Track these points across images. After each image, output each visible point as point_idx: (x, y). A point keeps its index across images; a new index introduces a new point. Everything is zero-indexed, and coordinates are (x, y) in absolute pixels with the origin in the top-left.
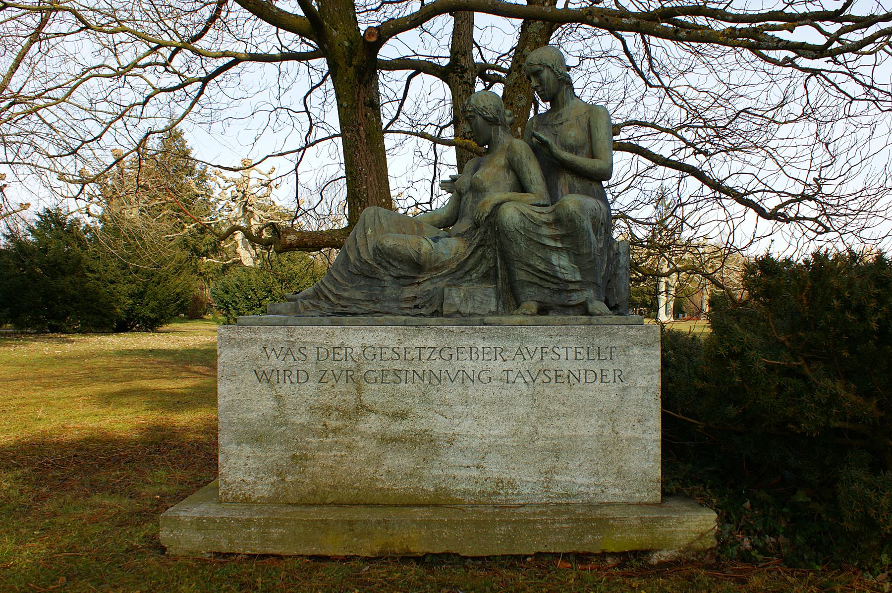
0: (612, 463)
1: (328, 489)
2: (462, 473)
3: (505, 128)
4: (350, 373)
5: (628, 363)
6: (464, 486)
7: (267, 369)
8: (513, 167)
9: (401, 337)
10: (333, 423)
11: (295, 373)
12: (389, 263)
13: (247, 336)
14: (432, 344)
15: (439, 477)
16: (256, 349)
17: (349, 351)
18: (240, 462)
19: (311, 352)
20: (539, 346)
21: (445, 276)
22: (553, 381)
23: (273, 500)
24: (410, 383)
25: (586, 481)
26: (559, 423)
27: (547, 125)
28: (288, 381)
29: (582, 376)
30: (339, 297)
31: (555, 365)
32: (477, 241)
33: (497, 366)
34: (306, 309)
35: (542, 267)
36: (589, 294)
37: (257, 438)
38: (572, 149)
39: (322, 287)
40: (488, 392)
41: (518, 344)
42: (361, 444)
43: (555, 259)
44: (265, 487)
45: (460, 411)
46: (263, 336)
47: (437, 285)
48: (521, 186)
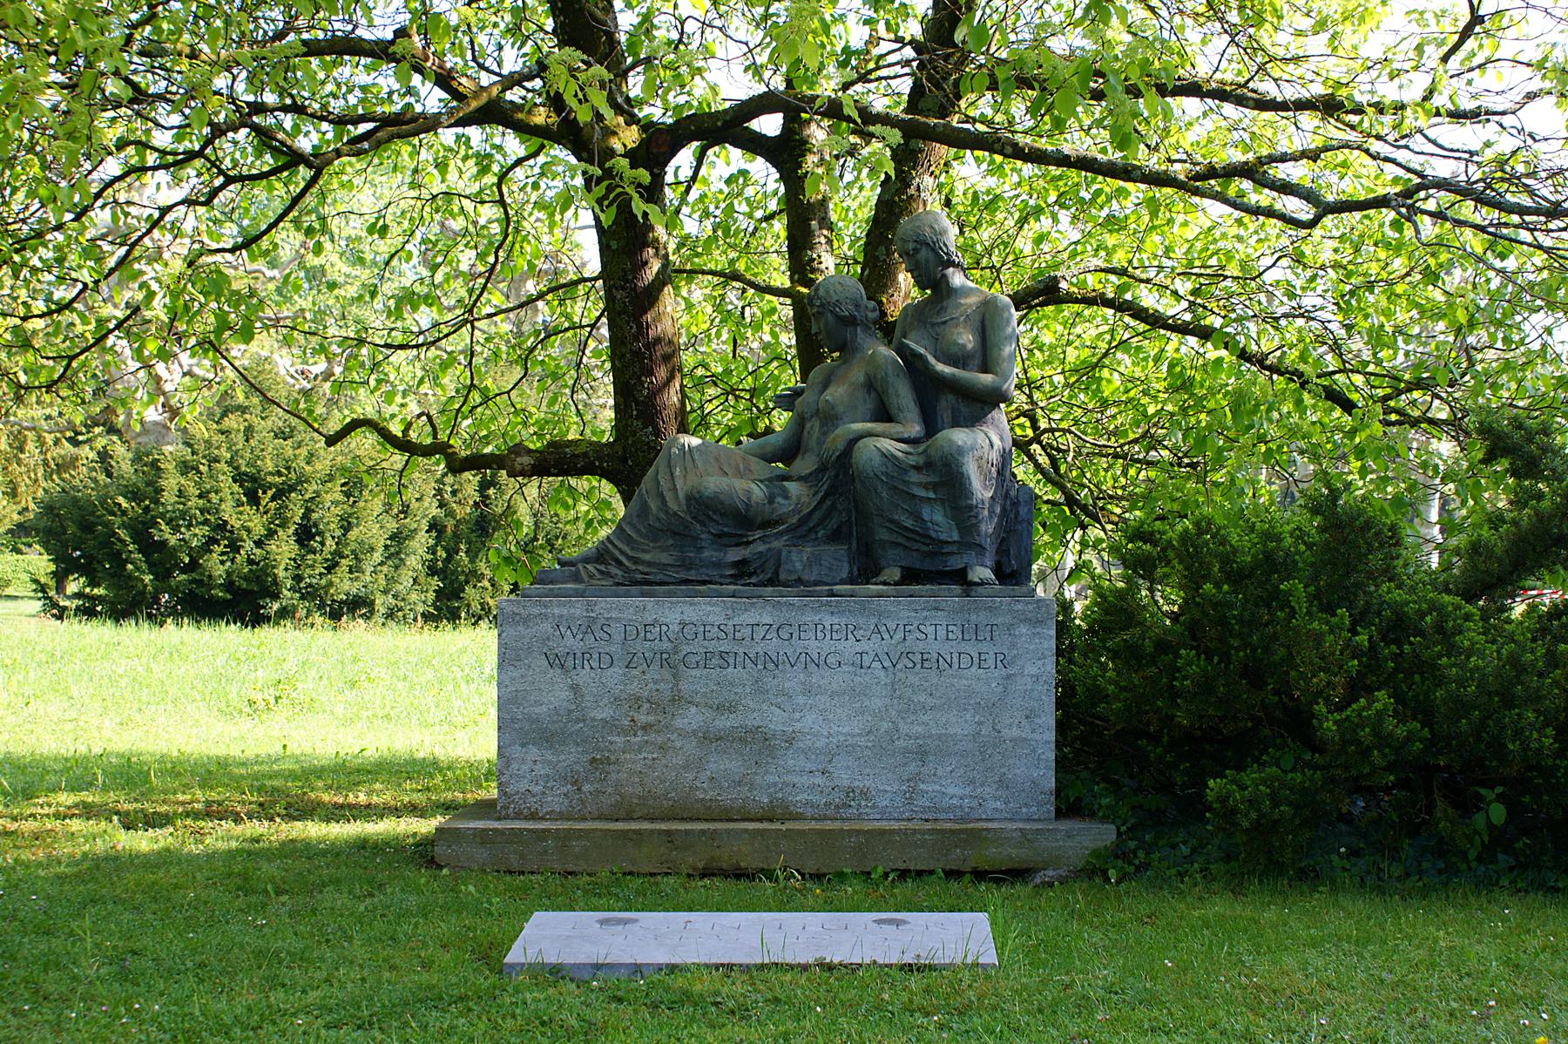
0: (992, 769)
1: (635, 801)
2: (805, 780)
3: (866, 328)
4: (665, 656)
5: (1013, 645)
6: (805, 795)
7: (560, 651)
9: (729, 612)
10: (642, 718)
11: (596, 656)
12: (709, 517)
13: (536, 611)
14: (768, 620)
15: (775, 784)
16: (547, 627)
17: (664, 628)
18: (525, 768)
19: (616, 631)
20: (901, 623)
21: (781, 534)
22: (919, 666)
24: (740, 668)
25: (958, 791)
26: (925, 718)
27: (925, 323)
28: (587, 666)
29: (955, 660)
30: (636, 561)
31: (921, 646)
32: (825, 487)
33: (849, 647)
34: (591, 577)
35: (909, 523)
38: (958, 360)
39: (610, 546)
40: (837, 680)
41: (876, 620)
42: (678, 744)
43: (926, 513)
44: (556, 799)
45: (801, 702)
46: (556, 611)
47: (772, 545)
48: (884, 414)
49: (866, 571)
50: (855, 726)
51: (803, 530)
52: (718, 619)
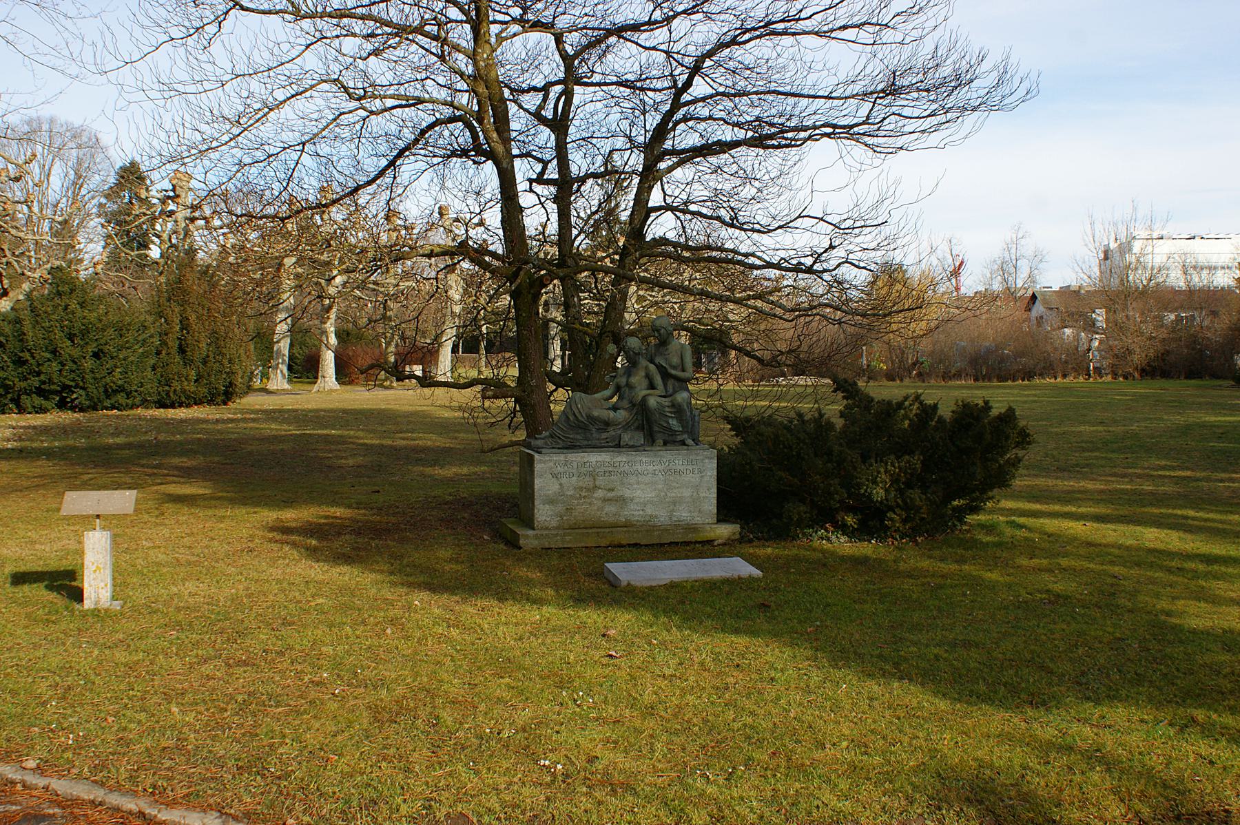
2: (637, 513)
8: (648, 376)
10: (583, 494)
16: (551, 464)
19: (575, 465)
23: (558, 528)
33: (651, 468)
36: (685, 436)
37: (551, 501)
38: (674, 368)
40: (647, 479)
43: (670, 421)
49: (651, 439)
50: (653, 494)
51: (627, 427)
52: (608, 460)
